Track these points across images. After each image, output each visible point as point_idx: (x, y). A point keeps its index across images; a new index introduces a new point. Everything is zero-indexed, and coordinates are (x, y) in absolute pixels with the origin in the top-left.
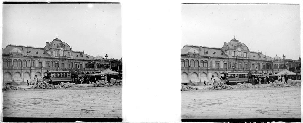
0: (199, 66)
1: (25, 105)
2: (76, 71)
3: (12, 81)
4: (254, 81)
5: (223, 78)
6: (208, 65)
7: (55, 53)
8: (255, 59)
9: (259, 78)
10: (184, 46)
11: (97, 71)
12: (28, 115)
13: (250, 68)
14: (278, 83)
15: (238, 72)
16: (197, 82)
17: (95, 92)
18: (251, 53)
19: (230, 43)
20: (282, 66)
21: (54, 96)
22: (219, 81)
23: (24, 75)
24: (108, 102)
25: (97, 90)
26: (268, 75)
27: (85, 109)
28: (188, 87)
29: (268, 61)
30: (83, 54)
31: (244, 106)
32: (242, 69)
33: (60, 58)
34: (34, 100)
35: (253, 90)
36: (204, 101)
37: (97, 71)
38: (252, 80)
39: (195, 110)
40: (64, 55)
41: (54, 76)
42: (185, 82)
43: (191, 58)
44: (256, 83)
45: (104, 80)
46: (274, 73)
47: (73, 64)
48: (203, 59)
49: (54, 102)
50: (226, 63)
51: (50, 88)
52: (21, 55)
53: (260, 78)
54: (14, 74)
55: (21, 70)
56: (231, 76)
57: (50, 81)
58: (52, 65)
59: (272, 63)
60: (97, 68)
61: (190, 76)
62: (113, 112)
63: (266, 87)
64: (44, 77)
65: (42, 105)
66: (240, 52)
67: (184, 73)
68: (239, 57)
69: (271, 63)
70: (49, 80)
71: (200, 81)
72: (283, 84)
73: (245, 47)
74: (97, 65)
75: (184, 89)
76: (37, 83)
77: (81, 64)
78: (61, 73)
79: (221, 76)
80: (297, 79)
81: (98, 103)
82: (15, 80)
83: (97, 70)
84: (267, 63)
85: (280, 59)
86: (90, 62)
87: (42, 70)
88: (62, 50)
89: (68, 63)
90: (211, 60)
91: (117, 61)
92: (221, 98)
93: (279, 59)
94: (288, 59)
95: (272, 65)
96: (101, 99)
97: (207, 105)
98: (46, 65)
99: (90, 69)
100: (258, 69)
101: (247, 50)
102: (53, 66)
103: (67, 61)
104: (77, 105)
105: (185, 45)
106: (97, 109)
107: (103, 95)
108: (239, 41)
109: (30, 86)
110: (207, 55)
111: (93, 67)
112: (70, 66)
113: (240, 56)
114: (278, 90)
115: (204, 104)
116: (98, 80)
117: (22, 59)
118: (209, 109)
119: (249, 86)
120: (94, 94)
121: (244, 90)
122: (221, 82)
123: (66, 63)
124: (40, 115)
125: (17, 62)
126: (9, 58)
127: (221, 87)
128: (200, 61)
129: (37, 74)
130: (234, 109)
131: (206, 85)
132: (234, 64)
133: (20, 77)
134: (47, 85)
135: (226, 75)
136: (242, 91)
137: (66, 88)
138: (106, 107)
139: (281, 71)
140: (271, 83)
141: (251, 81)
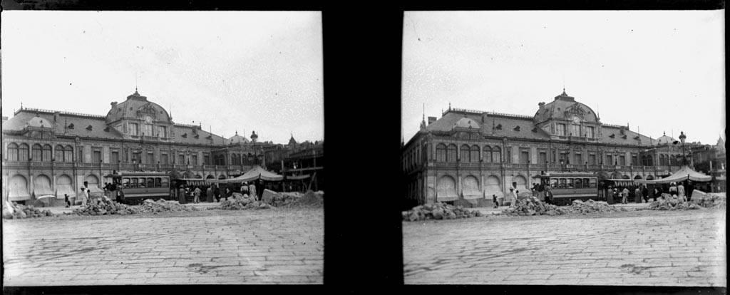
0: (482, 161)
1: (488, 253)
2: (182, 171)
3: (457, 196)
4: (183, 194)
5: (110, 188)
6: (75, 156)
7: (132, 128)
8: (613, 141)
9: (196, 187)
10: (16, 111)
11: (231, 173)
12: (495, 279)
13: (174, 163)
14: (669, 200)
15: (146, 172)
16: (49, 198)
17: (656, 223)
18: (603, 129)
19: (125, 104)
20: (250, 159)
21: (558, 232)
22: (100, 195)
23: (487, 182)
24: (686, 248)
25: (661, 217)
26: (644, 182)
27: (632, 263)
28: (28, 209)
29: (215, 147)
30: (626, 133)
31: (591, 255)
32: (584, 168)
33: (572, 140)
34: (511, 242)
35: (181, 217)
36: (66, 244)
37: (659, 174)
38: (179, 193)
39: (475, 265)
40: (153, 135)
41: (128, 183)
42: (21, 197)
43: (463, 140)
44: (617, 200)
45: (677, 193)
46: (230, 176)
47: (604, 155)
48: (62, 143)
49: (128, 247)
50: (116, 151)
51: (120, 214)
52: (50, 134)
53: (625, 189)
54: (34, 179)
55: (52, 168)
56: (128, 183)
57: (548, 197)
58: (125, 157)
59: (226, 151)
60: (661, 165)
61: (32, 184)
62: (699, 271)
63: (212, 209)
64: (534, 188)
65: (528, 254)
66: (578, 127)
67: (19, 175)
68: (574, 138)
69: (224, 151)
70: (545, 195)
71: (56, 195)
72: (681, 203)
73: (161, 112)
74: (232, 158)
75: (18, 214)
76: (517, 202)
77: (621, 156)
78: (146, 177)
79: (106, 183)
80: (284, 189)
81: (663, 249)
82: (464, 194)
83: (233, 170)
84: (212, 153)
85: (243, 142)
86: (643, 149)
87: (100, 170)
88: (148, 121)
89: (164, 153)
90: (82, 144)
91: (707, 148)
92: (105, 235)
93: (242, 141)
94: (691, 142)
95: (653, 156)
96: (668, 241)
97: (503, 252)
98: (110, 157)
99: (645, 167)
100: (620, 167)
101: (593, 120)
102: (127, 159)
103: (589, 148)
104: (180, 253)
105: (20, 107)
106: (660, 265)
107: (675, 231)
108: (575, 100)
109: (499, 208)
110: (499, 133)
111: (223, 163)
112: (596, 161)
113: (151, 135)
114: (673, 217)
115: (67, 250)
116: (234, 193)
117: (459, 142)
118: (508, 263)
119: (599, 206)
120: (653, 228)
121: (587, 217)
122: (105, 197)
123: (158, 151)
124: (524, 279)
125: (63, 151)
126: (449, 141)
127: (533, 209)
128: (437, 146)
129: (518, 180)
130: (568, 262)
131: (69, 203)
132: (563, 156)
133: (49, 186)
134: (113, 206)
135: (118, 180)
136: (155, 219)
137: (157, 213)
138: (680, 260)
139: (247, 170)
140: (224, 199)
141: (176, 195)
